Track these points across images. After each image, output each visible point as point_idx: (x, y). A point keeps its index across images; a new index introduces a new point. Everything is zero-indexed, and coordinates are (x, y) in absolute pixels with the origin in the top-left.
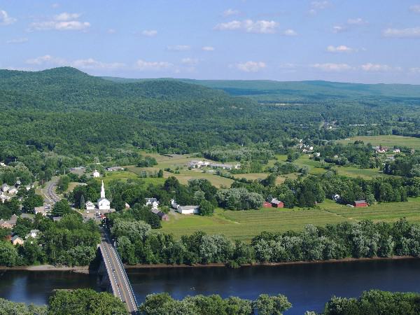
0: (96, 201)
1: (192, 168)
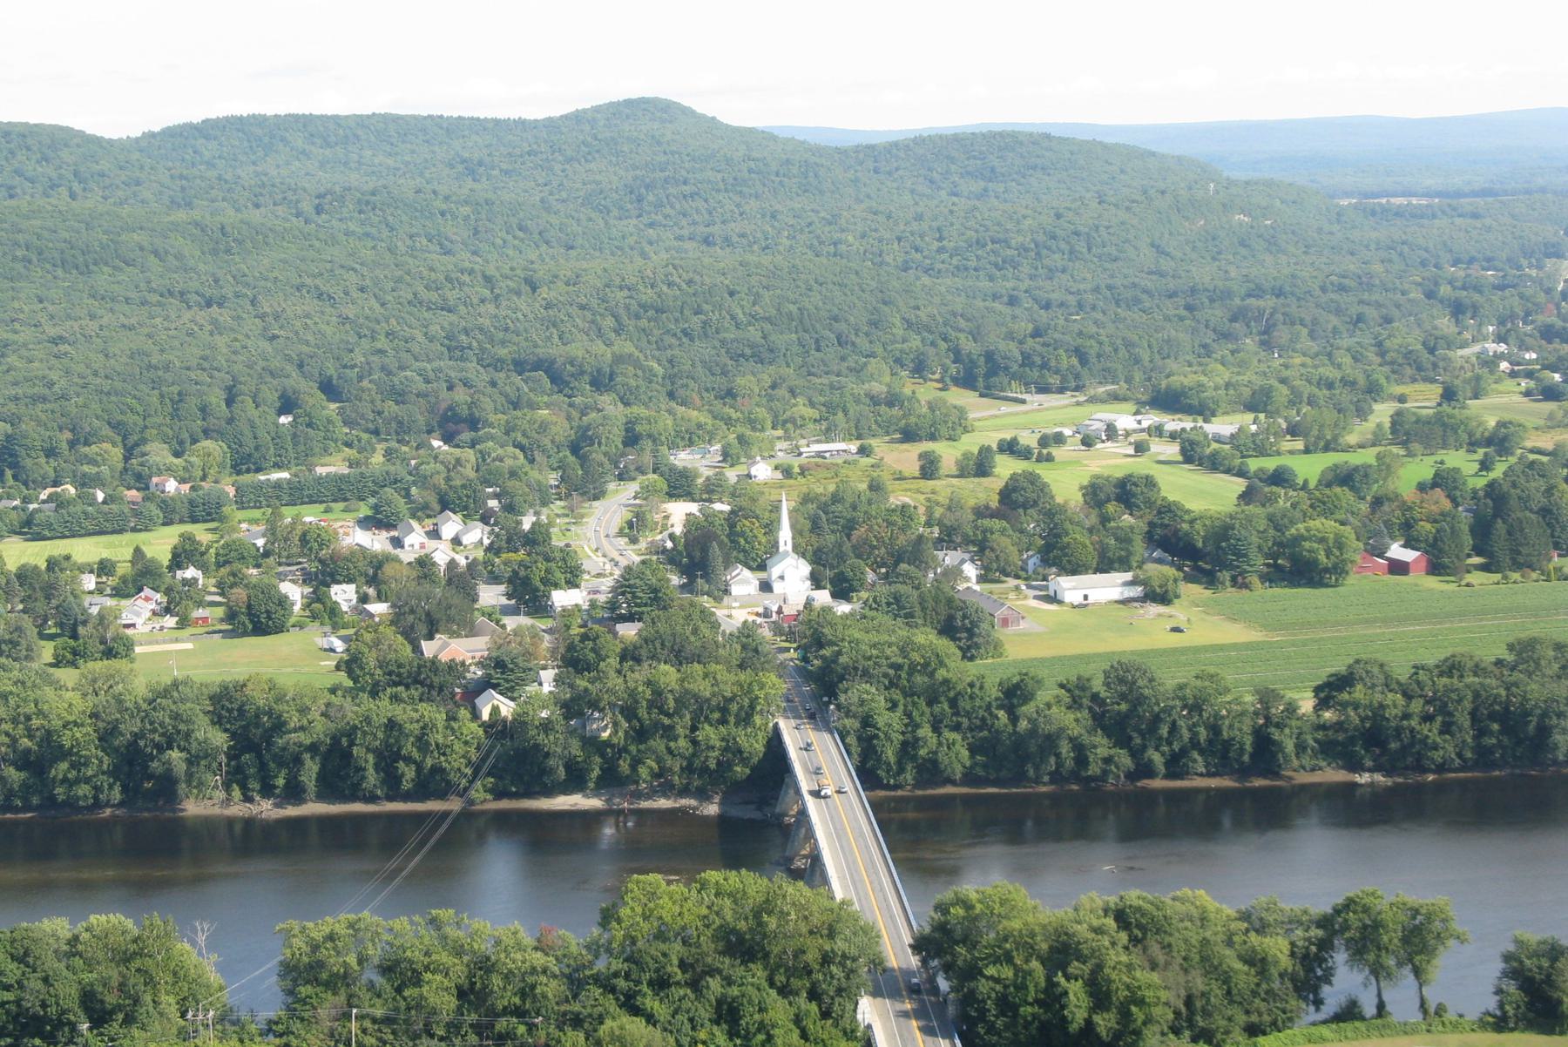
0: (762, 567)
1: (1091, 440)
